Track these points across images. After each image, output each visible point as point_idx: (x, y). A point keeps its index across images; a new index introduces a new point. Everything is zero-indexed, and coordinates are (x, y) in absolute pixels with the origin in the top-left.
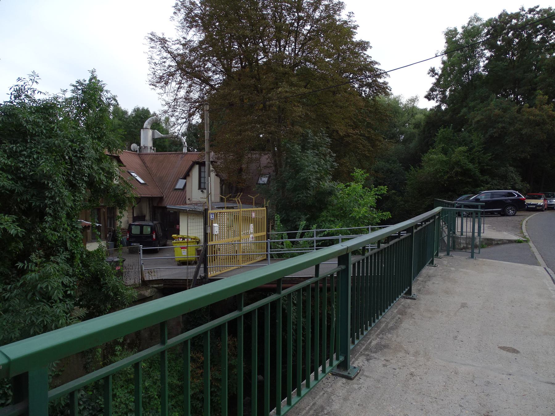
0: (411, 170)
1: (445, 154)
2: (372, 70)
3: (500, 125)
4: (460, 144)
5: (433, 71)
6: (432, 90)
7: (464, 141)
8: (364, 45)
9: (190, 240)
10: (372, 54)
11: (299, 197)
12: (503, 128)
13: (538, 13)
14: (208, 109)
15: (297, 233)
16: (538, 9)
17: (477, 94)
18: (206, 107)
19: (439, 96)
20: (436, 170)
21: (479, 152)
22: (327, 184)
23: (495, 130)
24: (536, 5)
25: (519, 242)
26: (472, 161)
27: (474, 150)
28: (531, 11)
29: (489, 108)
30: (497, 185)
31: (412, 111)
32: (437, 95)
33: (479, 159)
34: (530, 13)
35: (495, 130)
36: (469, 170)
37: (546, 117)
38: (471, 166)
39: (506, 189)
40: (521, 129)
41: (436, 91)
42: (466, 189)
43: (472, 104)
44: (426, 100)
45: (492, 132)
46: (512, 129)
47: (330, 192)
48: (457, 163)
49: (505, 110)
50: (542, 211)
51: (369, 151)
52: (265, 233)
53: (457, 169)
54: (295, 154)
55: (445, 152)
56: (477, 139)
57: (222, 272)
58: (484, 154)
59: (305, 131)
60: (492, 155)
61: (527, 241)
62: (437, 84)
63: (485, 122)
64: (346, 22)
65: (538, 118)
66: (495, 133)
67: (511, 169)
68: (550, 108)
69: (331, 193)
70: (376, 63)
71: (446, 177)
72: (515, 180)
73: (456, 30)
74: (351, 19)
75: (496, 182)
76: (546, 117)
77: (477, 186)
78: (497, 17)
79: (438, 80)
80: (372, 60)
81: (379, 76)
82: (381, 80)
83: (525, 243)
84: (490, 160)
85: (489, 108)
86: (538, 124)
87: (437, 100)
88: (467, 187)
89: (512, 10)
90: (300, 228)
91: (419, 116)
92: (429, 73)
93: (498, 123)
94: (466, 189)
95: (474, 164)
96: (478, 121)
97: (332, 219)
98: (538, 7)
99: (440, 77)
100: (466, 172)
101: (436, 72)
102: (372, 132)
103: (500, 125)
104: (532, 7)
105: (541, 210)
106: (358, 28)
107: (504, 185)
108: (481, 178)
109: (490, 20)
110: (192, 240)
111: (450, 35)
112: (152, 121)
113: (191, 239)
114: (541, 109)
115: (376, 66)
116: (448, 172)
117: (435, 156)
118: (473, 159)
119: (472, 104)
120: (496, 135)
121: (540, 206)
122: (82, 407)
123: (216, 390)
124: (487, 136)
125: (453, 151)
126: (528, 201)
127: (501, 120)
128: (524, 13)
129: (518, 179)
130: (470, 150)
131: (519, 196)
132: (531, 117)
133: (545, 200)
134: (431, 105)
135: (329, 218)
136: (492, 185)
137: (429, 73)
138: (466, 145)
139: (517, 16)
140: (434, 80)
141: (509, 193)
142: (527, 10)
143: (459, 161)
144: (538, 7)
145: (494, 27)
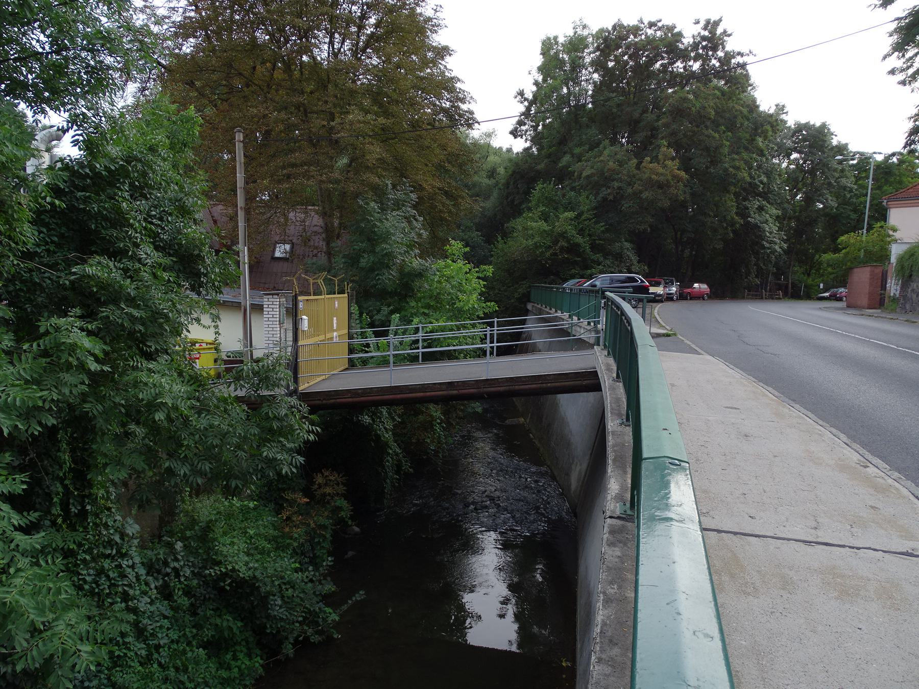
0: (498, 242)
1: (546, 221)
2: (452, 90)
3: (616, 184)
4: (566, 209)
5: (521, 93)
6: (521, 123)
7: (570, 203)
8: (443, 52)
9: (204, 346)
10: (453, 65)
11: (379, 279)
12: (620, 188)
13: (660, 29)
14: (242, 139)
15: (389, 330)
16: (660, 24)
17: (584, 137)
18: (239, 136)
19: (528, 133)
20: (536, 244)
21: (590, 220)
22: (416, 263)
23: (609, 191)
24: (658, 18)
25: (668, 335)
26: (581, 232)
27: (583, 217)
28: (651, 25)
29: (602, 158)
30: (609, 267)
31: (483, 149)
32: (527, 131)
33: (589, 230)
34: (650, 28)
35: (609, 191)
36: (578, 245)
37: (670, 178)
38: (579, 239)
39: (621, 272)
40: (641, 192)
41: (525, 124)
42: (573, 271)
43: (577, 151)
44: (511, 137)
45: (605, 193)
46: (630, 190)
47: (420, 273)
48: (563, 235)
49: (621, 164)
50: (662, 302)
51: (450, 212)
52: (346, 331)
53: (563, 243)
54: (372, 216)
55: (545, 217)
56: (586, 202)
57: (311, 384)
58: (596, 223)
59: (382, 181)
60: (605, 225)
61: (675, 334)
62: (527, 114)
63: (596, 178)
64: (430, 19)
65: (662, 178)
66: (609, 194)
67: (627, 245)
68: (675, 165)
69: (420, 274)
70: (459, 80)
71: (548, 254)
72: (631, 260)
73: (556, 38)
74: (438, 14)
75: (609, 263)
76: (670, 178)
77: (587, 267)
78: (610, 28)
79: (528, 109)
80: (452, 76)
81: (463, 101)
82: (464, 107)
83: (674, 337)
84: (603, 232)
85: (602, 158)
86: (661, 186)
87: (526, 139)
88: (574, 268)
89: (630, 20)
90: (392, 323)
91: (492, 158)
92: (516, 97)
93: (613, 180)
94: (573, 271)
95: (583, 237)
96: (588, 177)
97: (426, 311)
98: (660, 21)
99: (531, 103)
100: (573, 248)
101: (526, 96)
102: (454, 184)
103: (616, 184)
104: (653, 20)
105: (661, 301)
106: (446, 28)
107: (618, 266)
108: (593, 257)
109: (602, 31)
110: (209, 346)
111: (548, 46)
112: (49, 137)
113: (207, 344)
114: (665, 167)
115: (458, 85)
116: (550, 247)
117: (534, 224)
118: (582, 230)
119: (577, 151)
120: (611, 197)
121: (660, 295)
122: (182, 563)
123: (321, 540)
124: (599, 198)
125: (557, 217)
126: (652, 290)
127: (616, 177)
128: (643, 25)
129: (634, 258)
130: (580, 215)
131: (642, 281)
132: (653, 176)
133: (665, 287)
134: (519, 145)
135: (422, 310)
136: (604, 266)
137: (516, 97)
138: (573, 209)
139: (635, 30)
140: (522, 108)
141: (629, 278)
142: (646, 22)
143: (566, 232)
144: (660, 21)
145: (606, 39)
